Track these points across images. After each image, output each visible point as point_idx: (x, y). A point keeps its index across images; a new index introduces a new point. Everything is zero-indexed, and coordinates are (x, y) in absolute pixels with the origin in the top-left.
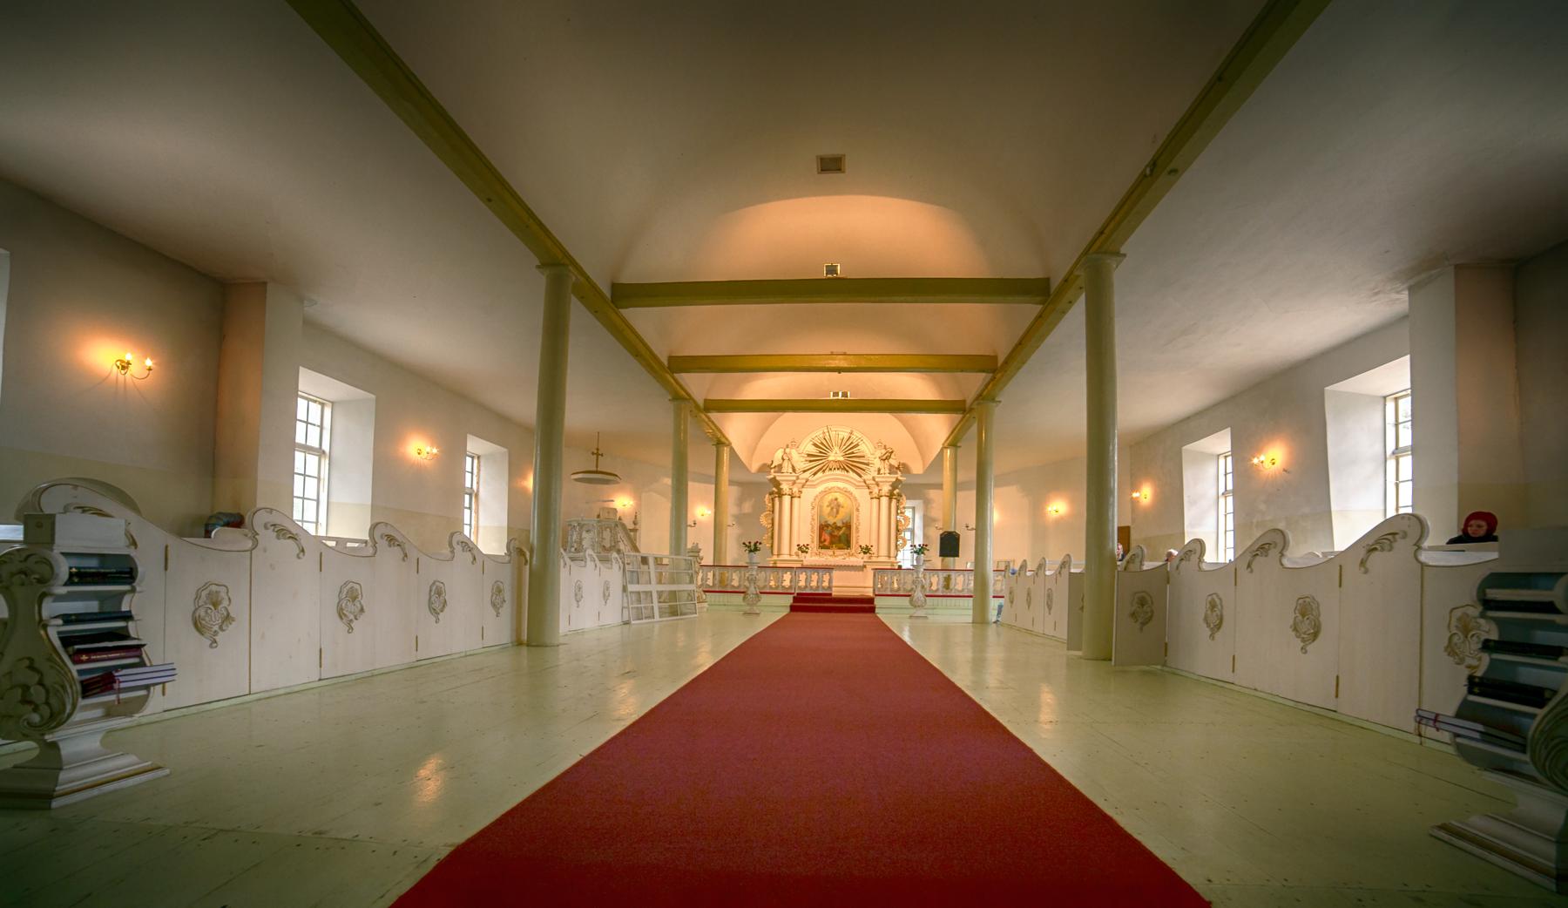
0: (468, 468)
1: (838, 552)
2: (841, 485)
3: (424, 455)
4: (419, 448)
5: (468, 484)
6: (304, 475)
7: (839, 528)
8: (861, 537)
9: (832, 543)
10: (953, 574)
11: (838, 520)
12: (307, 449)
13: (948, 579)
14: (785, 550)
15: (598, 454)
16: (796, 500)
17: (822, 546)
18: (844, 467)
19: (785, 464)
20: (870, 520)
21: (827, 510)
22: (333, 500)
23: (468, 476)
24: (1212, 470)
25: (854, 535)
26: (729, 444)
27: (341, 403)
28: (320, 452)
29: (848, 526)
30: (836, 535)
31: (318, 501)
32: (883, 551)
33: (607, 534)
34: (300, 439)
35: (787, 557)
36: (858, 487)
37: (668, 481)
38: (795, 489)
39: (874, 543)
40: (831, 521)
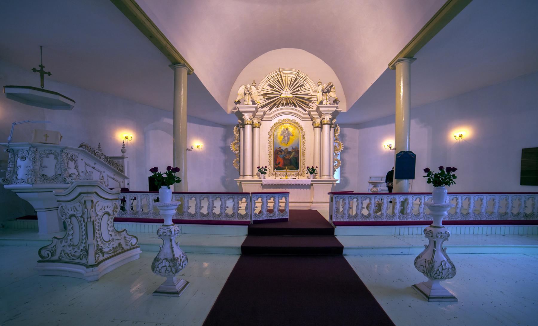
1: (290, 172)
2: (291, 118)
7: (290, 153)
8: (307, 160)
9: (285, 165)
10: (410, 197)
11: (289, 147)
14: (248, 172)
16: (256, 130)
17: (278, 167)
18: (290, 102)
20: (317, 145)
21: (280, 138)
26: (185, 64)
29: (297, 151)
30: (287, 159)
32: (326, 172)
35: (249, 178)
36: (303, 119)
38: (256, 121)
39: (317, 164)
40: (284, 147)
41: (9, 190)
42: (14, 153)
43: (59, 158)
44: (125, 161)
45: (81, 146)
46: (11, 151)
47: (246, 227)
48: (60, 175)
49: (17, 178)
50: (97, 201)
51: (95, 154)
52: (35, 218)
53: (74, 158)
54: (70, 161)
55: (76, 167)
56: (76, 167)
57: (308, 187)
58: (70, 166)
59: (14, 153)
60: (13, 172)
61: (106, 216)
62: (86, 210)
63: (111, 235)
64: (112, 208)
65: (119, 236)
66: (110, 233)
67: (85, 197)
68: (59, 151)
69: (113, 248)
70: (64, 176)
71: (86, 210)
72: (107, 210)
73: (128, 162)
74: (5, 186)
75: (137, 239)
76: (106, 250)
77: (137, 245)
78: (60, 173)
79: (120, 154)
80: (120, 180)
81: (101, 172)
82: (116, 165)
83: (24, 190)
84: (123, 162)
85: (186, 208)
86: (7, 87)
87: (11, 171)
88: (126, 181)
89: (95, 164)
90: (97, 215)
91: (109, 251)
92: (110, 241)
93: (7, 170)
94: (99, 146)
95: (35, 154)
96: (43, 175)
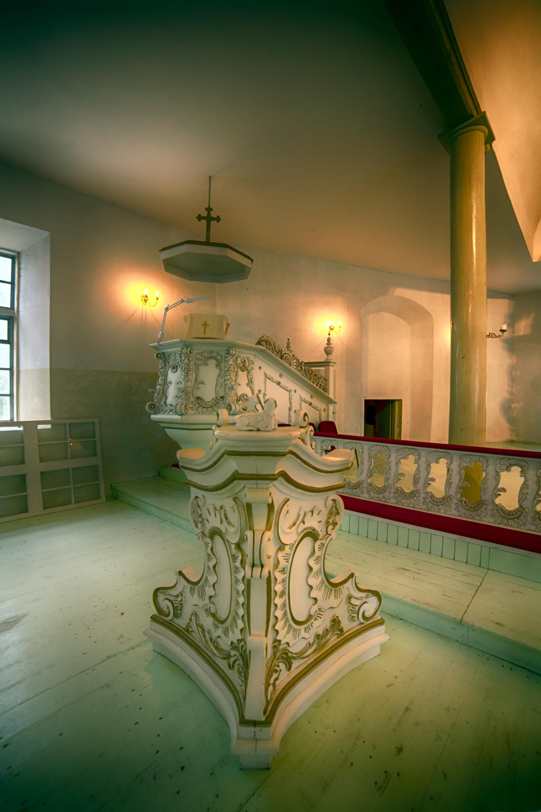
41: (157, 422)
42: (165, 361)
43: (222, 365)
44: (331, 369)
45: (259, 343)
46: (162, 356)
48: (222, 397)
49: (165, 402)
50: (284, 497)
51: (282, 357)
53: (247, 364)
54: (240, 372)
55: (250, 383)
56: (250, 383)
58: (239, 380)
59: (165, 361)
60: (163, 392)
61: (308, 541)
62: (249, 534)
63: (316, 599)
64: (323, 517)
65: (336, 596)
66: (314, 594)
67: (250, 493)
68: (223, 353)
69: (318, 636)
70: (229, 400)
71: (249, 534)
72: (312, 522)
73: (335, 371)
74: (152, 416)
75: (380, 600)
76: (296, 647)
77: (378, 617)
78: (223, 395)
79: (321, 357)
80: (321, 405)
81: (290, 391)
82: (315, 377)
83: (173, 425)
84: (327, 371)
85: (489, 492)
86: (164, 249)
87: (160, 389)
88: (331, 408)
89: (281, 376)
90: (282, 547)
91: (305, 650)
92: (310, 617)
93: (155, 389)
94: (288, 344)
95: (189, 360)
96: (198, 398)
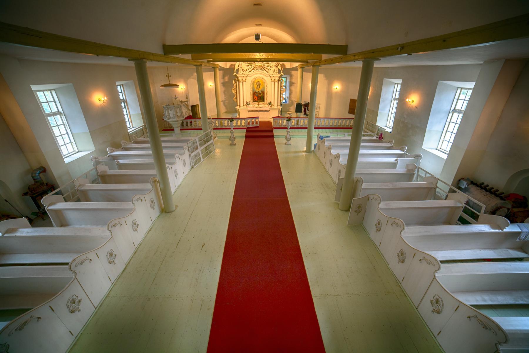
0: (120, 91)
3: (102, 102)
4: (99, 98)
5: (121, 98)
6: (58, 126)
7: (260, 94)
9: (258, 100)
12: (53, 114)
13: (298, 121)
14: (242, 105)
15: (168, 76)
19: (240, 69)
21: (256, 86)
22: (73, 132)
23: (120, 94)
24: (392, 89)
25: (266, 96)
27: (57, 88)
28: (58, 113)
29: (263, 93)
30: (259, 97)
31: (67, 134)
33: (178, 110)
34: (47, 110)
35: (242, 108)
37: (196, 74)
38: (244, 79)
39: (273, 101)
40: (257, 91)
47: (245, 130)
52: (173, 130)
57: (268, 111)
